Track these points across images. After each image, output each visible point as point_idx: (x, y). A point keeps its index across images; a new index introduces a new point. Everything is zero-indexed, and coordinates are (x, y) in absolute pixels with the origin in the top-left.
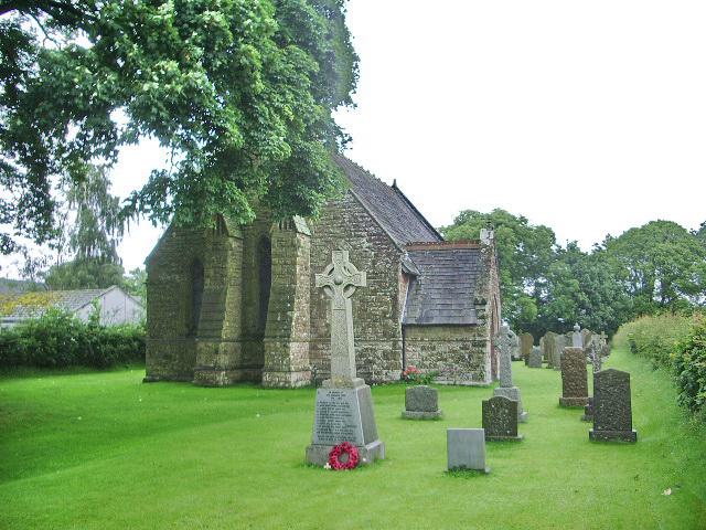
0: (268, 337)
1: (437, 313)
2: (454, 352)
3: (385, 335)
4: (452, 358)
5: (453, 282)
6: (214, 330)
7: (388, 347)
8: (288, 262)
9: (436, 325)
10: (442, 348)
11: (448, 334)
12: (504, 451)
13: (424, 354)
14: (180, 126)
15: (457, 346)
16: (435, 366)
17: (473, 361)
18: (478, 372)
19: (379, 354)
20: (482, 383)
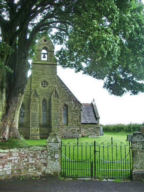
0: (53, 126)
1: (88, 120)
2: (92, 130)
3: (78, 125)
4: (92, 131)
5: (89, 113)
6: (55, 65)
7: (78, 128)
8: (57, 106)
9: (89, 123)
10: (90, 129)
11: (91, 125)
12: (103, 85)
13: (85, 130)
14: (3, 180)
15: (93, 128)
16: (88, 133)
17: (97, 132)
18: (98, 134)
19: (77, 130)
20: (98, 137)
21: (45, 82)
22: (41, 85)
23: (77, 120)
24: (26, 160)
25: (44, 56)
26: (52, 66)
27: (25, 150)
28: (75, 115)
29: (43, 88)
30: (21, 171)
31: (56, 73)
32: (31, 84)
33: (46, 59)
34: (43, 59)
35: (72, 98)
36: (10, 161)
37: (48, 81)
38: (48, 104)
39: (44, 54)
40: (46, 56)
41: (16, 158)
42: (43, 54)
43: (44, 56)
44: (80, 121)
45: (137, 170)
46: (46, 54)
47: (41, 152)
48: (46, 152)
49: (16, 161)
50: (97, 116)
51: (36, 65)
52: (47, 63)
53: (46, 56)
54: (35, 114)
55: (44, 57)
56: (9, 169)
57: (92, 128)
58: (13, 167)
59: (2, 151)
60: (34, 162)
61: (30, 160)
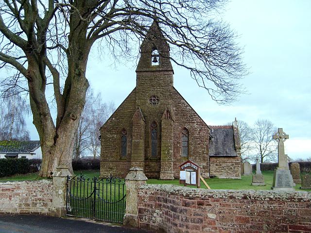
2: (229, 166)
7: (205, 164)
10: (224, 165)
11: (226, 159)
17: (236, 169)
21: (154, 96)
22: (149, 102)
23: (203, 151)
24: (35, 194)
25: (155, 59)
26: (166, 73)
27: (33, 184)
28: (200, 143)
29: (152, 106)
30: (29, 206)
31: (172, 82)
32: (135, 101)
33: (157, 64)
34: (153, 64)
35: (195, 118)
36: (18, 194)
37: (159, 95)
38: (158, 127)
39: (155, 56)
40: (158, 58)
41: (24, 191)
42: (154, 56)
43: (155, 59)
44: (207, 154)
45: (129, 214)
46: (158, 56)
47: (49, 186)
48: (52, 186)
49: (24, 195)
50: (236, 146)
51: (144, 74)
52: (158, 69)
53: (158, 58)
54: (138, 143)
55: (155, 61)
56: (17, 202)
57: (228, 164)
58: (21, 201)
59: (1, 183)
60: (41, 197)
61: (39, 194)
